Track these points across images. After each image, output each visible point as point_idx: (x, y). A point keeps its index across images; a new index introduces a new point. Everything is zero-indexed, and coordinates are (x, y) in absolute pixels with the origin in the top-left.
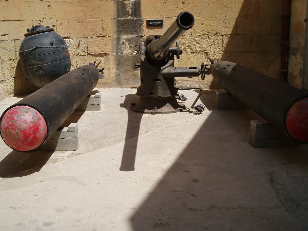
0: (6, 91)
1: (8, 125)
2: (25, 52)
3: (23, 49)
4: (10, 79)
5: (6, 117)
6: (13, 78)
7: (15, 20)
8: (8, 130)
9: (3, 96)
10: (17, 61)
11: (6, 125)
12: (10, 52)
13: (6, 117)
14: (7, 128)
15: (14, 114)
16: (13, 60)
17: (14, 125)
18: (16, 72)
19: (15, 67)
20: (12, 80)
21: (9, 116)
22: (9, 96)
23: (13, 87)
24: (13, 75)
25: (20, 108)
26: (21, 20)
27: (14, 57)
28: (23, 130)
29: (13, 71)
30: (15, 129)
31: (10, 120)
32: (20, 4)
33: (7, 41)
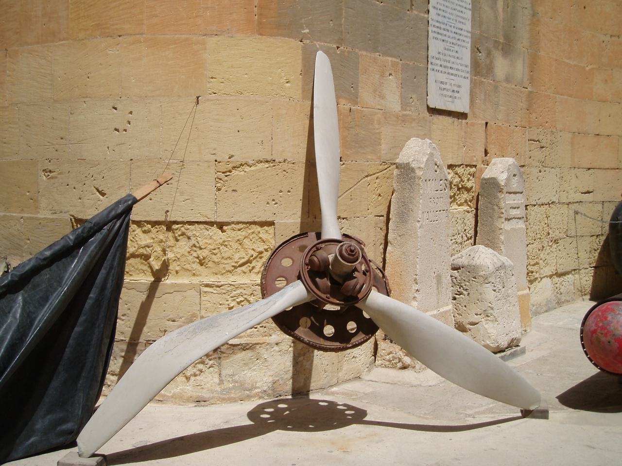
0: (578, 289)
1: (596, 328)
2: (619, 226)
3: (617, 218)
4: (587, 269)
5: (594, 316)
6: (593, 268)
7: (608, 169)
8: (596, 334)
9: (573, 296)
10: (603, 238)
11: (594, 328)
12: (593, 222)
13: (594, 316)
14: (595, 332)
15: (607, 312)
16: (597, 236)
17: (606, 328)
18: (599, 257)
19: (598, 249)
20: (591, 270)
21: (600, 314)
22: (581, 298)
23: (591, 283)
24: (593, 262)
25: (618, 304)
26: (617, 169)
27: (598, 231)
28: (619, 338)
29: (594, 255)
30: (606, 334)
31: (601, 320)
32: (619, 140)
33: (590, 202)
